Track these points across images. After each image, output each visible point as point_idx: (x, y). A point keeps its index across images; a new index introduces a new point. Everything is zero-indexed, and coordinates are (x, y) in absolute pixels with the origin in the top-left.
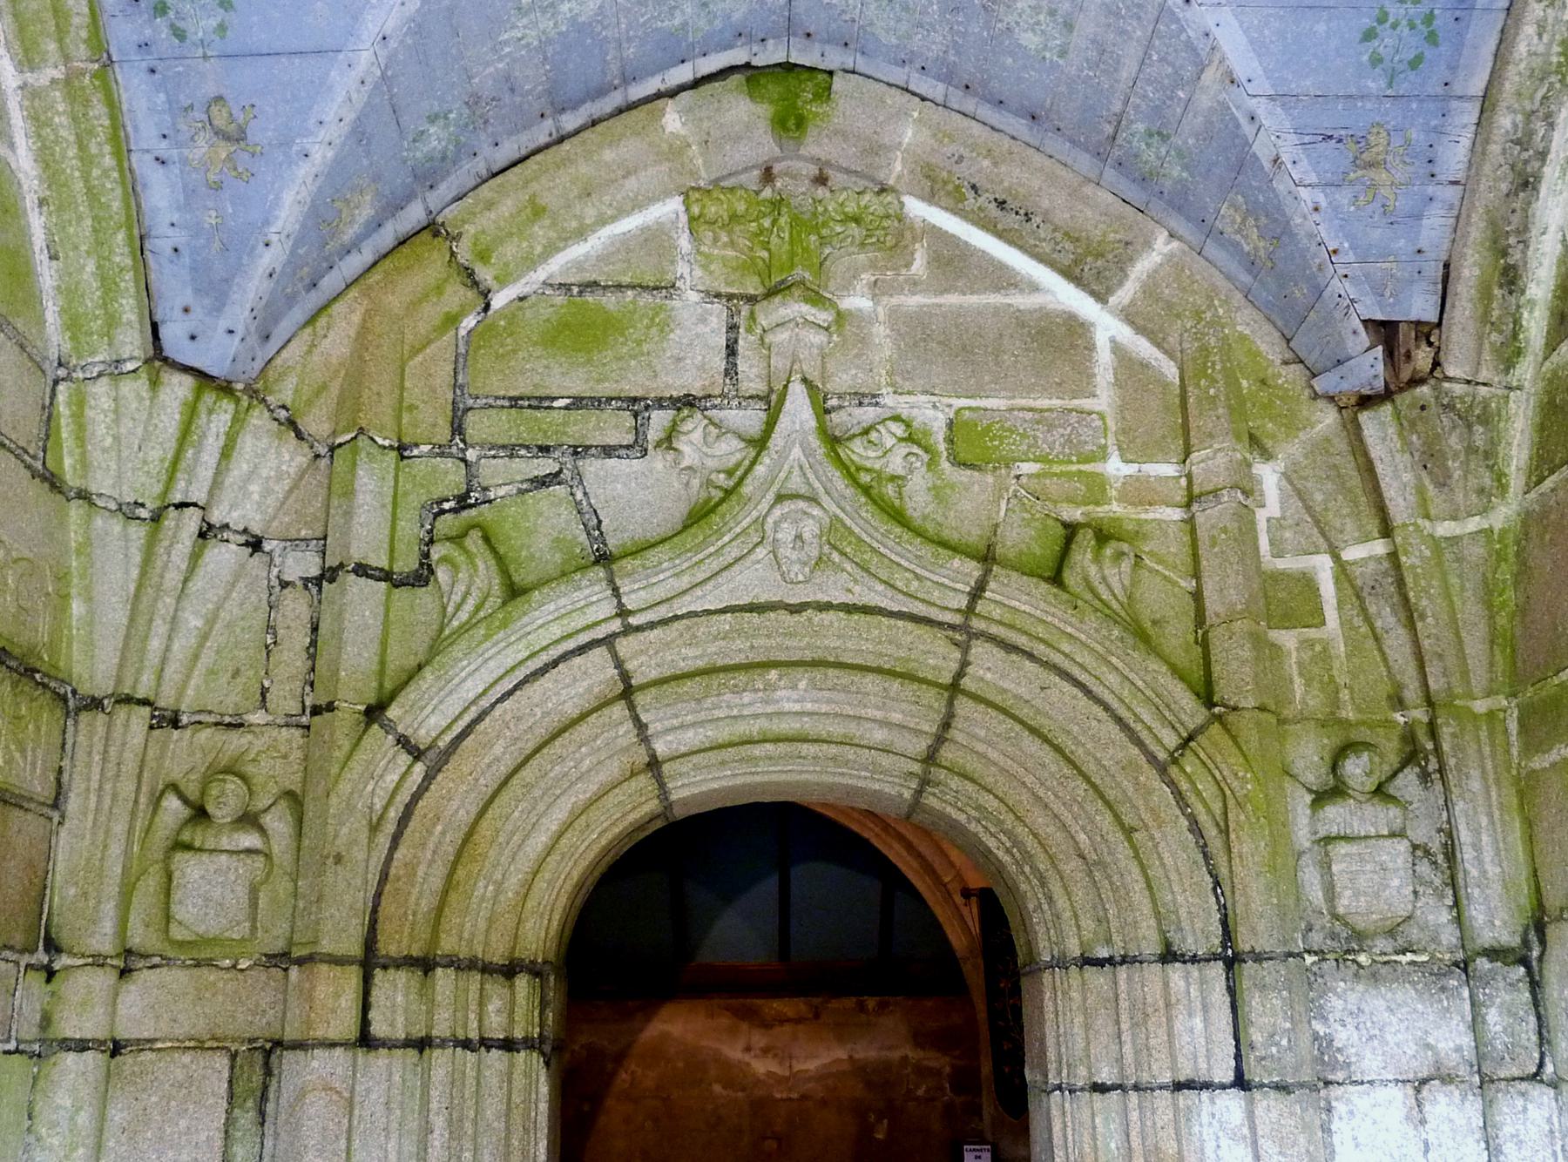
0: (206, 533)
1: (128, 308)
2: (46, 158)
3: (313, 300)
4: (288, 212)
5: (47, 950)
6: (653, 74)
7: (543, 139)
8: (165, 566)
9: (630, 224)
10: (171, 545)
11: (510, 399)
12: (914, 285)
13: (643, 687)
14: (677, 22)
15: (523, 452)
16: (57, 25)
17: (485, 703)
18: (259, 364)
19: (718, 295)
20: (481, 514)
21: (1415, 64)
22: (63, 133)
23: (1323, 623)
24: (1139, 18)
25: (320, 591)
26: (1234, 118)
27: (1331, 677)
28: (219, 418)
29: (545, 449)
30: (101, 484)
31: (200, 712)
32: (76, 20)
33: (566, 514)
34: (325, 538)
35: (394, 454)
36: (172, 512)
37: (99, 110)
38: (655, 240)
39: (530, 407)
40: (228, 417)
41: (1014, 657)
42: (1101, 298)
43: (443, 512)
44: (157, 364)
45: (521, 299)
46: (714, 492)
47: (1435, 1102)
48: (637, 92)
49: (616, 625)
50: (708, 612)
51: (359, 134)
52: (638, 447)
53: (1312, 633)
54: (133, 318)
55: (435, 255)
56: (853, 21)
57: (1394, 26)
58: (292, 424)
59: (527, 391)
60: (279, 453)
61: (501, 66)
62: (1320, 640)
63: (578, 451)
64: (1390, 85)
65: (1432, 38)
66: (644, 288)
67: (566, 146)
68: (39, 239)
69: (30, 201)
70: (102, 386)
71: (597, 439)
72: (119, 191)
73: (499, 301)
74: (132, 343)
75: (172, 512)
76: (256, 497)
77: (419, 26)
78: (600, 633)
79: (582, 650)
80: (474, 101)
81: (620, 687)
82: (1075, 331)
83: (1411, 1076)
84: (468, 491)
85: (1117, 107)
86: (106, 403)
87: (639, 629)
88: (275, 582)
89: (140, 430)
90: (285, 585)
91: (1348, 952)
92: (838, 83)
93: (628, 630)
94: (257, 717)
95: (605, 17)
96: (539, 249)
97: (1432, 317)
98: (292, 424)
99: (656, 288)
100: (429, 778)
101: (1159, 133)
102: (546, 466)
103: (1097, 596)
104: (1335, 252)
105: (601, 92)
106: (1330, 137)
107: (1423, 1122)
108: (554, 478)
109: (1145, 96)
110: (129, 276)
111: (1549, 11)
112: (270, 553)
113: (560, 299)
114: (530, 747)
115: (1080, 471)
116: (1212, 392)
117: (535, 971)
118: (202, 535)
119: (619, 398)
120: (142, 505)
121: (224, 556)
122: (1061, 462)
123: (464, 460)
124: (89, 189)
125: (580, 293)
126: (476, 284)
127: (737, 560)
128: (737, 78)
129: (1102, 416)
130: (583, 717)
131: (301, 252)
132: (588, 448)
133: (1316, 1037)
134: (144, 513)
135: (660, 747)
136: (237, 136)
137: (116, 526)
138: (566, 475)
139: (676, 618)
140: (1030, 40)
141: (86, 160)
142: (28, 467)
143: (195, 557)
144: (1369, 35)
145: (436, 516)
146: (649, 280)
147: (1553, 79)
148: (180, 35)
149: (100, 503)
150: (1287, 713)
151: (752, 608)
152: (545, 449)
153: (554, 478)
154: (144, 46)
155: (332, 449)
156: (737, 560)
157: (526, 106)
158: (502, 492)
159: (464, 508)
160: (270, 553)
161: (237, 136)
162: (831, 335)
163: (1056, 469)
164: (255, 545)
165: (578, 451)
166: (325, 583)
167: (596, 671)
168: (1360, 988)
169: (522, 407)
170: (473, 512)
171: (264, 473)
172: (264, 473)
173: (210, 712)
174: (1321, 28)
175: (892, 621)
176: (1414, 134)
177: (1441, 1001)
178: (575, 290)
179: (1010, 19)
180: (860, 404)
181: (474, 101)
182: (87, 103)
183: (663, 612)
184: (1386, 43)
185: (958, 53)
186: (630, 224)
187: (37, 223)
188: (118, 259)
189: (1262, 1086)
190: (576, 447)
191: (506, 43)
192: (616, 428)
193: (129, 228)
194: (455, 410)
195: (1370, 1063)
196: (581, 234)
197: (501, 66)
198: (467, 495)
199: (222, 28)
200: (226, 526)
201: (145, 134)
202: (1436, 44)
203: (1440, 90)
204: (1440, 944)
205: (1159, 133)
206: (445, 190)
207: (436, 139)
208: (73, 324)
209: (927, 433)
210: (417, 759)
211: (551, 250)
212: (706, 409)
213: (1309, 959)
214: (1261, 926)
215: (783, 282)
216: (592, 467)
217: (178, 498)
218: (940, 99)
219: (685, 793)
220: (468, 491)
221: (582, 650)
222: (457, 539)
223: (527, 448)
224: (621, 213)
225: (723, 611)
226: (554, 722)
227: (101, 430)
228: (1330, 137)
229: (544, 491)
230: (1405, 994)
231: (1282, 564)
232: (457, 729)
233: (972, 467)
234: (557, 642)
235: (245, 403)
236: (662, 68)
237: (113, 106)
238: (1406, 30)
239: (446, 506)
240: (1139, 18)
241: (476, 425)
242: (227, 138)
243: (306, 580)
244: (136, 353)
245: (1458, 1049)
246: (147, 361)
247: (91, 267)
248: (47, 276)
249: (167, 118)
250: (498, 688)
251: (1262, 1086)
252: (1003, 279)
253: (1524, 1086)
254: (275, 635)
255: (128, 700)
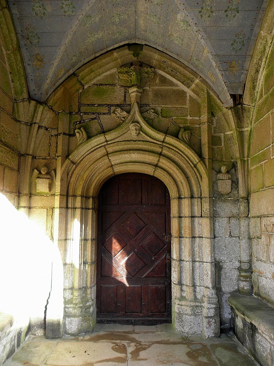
0: (40, 127)
1: (25, 90)
3: (55, 87)
4: (51, 74)
5: (18, 193)
6: (112, 46)
7: (93, 58)
8: (33, 133)
9: (108, 73)
10: (34, 130)
11: (88, 104)
12: (156, 85)
13: (110, 153)
14: (116, 37)
15: (90, 114)
16: (11, 42)
17: (84, 156)
18: (46, 99)
19: (123, 86)
20: (83, 124)
21: (240, 49)
22: (13, 61)
23: (221, 145)
24: (194, 40)
25: (58, 137)
26: (209, 58)
27: (222, 154)
28: (41, 108)
29: (93, 113)
30: (22, 119)
31: (39, 156)
32: (14, 41)
33: (97, 124)
34: (58, 128)
35: (69, 114)
36: (33, 124)
37: (19, 56)
38: (112, 76)
39: (91, 106)
40: (42, 108)
42: (188, 87)
43: (77, 124)
44: (30, 99)
45: (89, 87)
46: (122, 121)
47: (232, 220)
48: (109, 49)
49: (105, 143)
50: (120, 141)
51: (62, 59)
52: (109, 113)
53: (219, 146)
54: (26, 91)
55: (75, 79)
56: (147, 36)
57: (237, 43)
58: (52, 109)
59: (91, 103)
61: (85, 46)
62: (221, 148)
63: (99, 114)
64: (236, 53)
65: (243, 45)
66: (110, 85)
67: (97, 59)
70: (21, 103)
71: (102, 112)
72: (22, 70)
73: (86, 87)
74: (25, 95)
75: (33, 124)
76: (46, 121)
77: (71, 41)
78: (103, 145)
79: (100, 147)
80: (81, 53)
81: (106, 153)
82: (184, 93)
83: (229, 216)
84: (81, 120)
85: (191, 54)
86: (22, 106)
87: (109, 144)
88: (50, 135)
89: (27, 110)
90: (52, 136)
91: (220, 197)
92: (144, 47)
93: (108, 144)
94: (48, 158)
95: (103, 37)
96: (92, 78)
97: (242, 94)
98: (52, 109)
99: (112, 85)
100: (76, 167)
101: (198, 60)
102: (94, 116)
103: (184, 140)
104: (225, 82)
105: (102, 50)
106: (225, 62)
107: (230, 223)
108: (95, 118)
109: (195, 53)
110: (25, 85)
111: (263, 41)
112: (49, 131)
113: (96, 87)
114: (92, 163)
115: (183, 118)
116: (205, 105)
117: (196, 164)
118: (38, 128)
119: (106, 105)
120: (29, 123)
121: (42, 131)
122: (180, 117)
123: (80, 115)
125: (99, 86)
126: (82, 84)
127: (125, 133)
128: (126, 47)
129: (187, 109)
130: (100, 158)
131: (52, 80)
132: (101, 113)
133: (214, 210)
134: (29, 124)
135: (113, 163)
136: (41, 61)
137: (25, 126)
138: (97, 118)
139: (115, 142)
140: (176, 42)
141: (17, 65)
142: (11, 117)
143: (38, 131)
144: (232, 44)
145: (76, 125)
146: (111, 83)
147: (262, 53)
148: (31, 43)
150: (214, 159)
151: (127, 141)
152: (93, 113)
153: (95, 118)
154: (25, 45)
155: (59, 113)
156: (125, 133)
157: (90, 53)
158: (86, 121)
159: (80, 123)
160: (49, 131)
161: (41, 61)
162: (142, 94)
163: (179, 118)
164: (47, 129)
165: (99, 114)
166: (58, 136)
167: (103, 151)
168: (222, 203)
169: (90, 106)
170: (82, 124)
171: (48, 117)
172: (48, 117)
173: (41, 157)
174: (224, 43)
175: (151, 143)
176: (240, 62)
177: (234, 205)
178: (99, 85)
179: (173, 38)
180: (146, 106)
181: (81, 53)
182: (17, 56)
183: (113, 141)
184: (235, 46)
185: (164, 43)
186: (108, 73)
189: (204, 217)
190: (99, 113)
191: (86, 43)
192: (105, 110)
193: (24, 76)
194: (79, 106)
195: (222, 214)
196: (99, 75)
197: (85, 46)
198: (81, 121)
199: (38, 42)
201: (26, 59)
202: (244, 46)
203: (244, 54)
204: (235, 196)
205: (198, 60)
206: (76, 67)
207: (74, 59)
209: (158, 111)
210: (74, 164)
211: (94, 78)
212: (120, 107)
213: (214, 198)
214: (206, 193)
215: (134, 84)
216: (101, 116)
217: (34, 122)
218: (162, 51)
219: (117, 171)
220: (81, 120)
221: (100, 147)
222: (79, 129)
223: (91, 113)
224: (106, 71)
225: (123, 141)
226: (96, 159)
228: (225, 62)
229: (94, 121)
230: (229, 204)
231: (215, 135)
232: (80, 160)
233: (165, 117)
234: (96, 146)
235: (44, 106)
236: (113, 45)
237: (21, 55)
238: (239, 44)
239: (78, 123)
240: (194, 40)
241: (83, 109)
242: (40, 61)
243: (55, 135)
245: (237, 212)
246: (28, 99)
249: (30, 57)
250: (86, 153)
251: (204, 217)
252: (172, 84)
253: (245, 218)
254: (50, 144)
255: (28, 155)
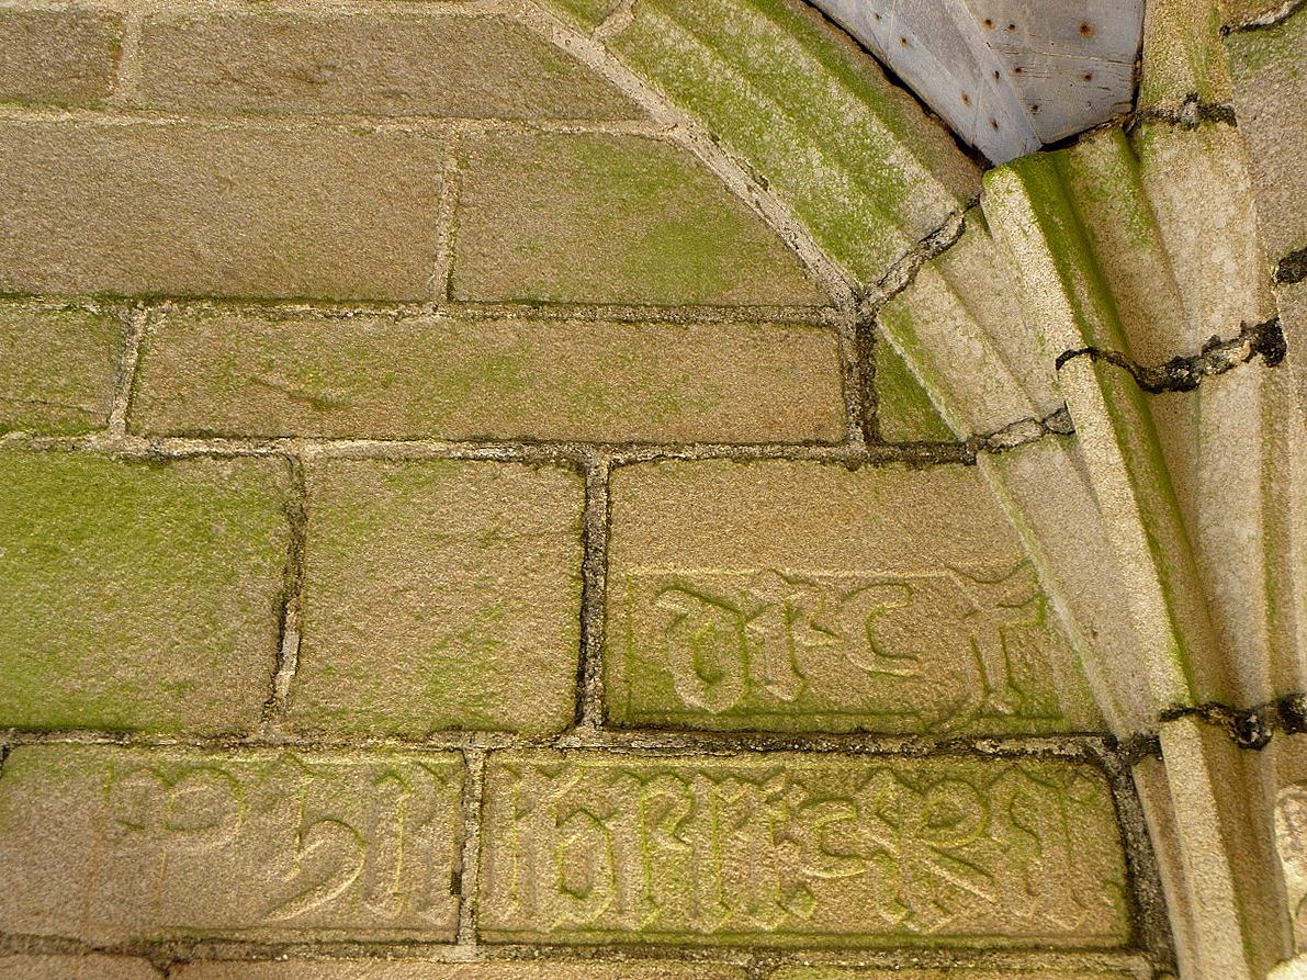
2: (687, 93)
41: (898, 89)
54: (916, 168)
60: (1223, 174)
68: (738, 180)
69: (701, 149)
86: (947, 301)
124: (754, 77)
149: (1008, 440)
187: (730, 170)
188: (850, 118)
200: (1215, 343)
208: (837, 240)
227: (959, 341)
244: (950, 207)
247: (815, 155)
248: (779, 211)
